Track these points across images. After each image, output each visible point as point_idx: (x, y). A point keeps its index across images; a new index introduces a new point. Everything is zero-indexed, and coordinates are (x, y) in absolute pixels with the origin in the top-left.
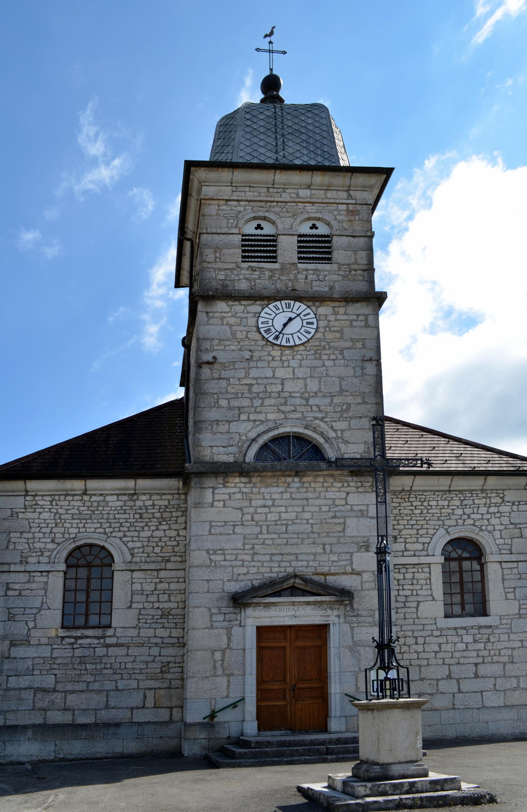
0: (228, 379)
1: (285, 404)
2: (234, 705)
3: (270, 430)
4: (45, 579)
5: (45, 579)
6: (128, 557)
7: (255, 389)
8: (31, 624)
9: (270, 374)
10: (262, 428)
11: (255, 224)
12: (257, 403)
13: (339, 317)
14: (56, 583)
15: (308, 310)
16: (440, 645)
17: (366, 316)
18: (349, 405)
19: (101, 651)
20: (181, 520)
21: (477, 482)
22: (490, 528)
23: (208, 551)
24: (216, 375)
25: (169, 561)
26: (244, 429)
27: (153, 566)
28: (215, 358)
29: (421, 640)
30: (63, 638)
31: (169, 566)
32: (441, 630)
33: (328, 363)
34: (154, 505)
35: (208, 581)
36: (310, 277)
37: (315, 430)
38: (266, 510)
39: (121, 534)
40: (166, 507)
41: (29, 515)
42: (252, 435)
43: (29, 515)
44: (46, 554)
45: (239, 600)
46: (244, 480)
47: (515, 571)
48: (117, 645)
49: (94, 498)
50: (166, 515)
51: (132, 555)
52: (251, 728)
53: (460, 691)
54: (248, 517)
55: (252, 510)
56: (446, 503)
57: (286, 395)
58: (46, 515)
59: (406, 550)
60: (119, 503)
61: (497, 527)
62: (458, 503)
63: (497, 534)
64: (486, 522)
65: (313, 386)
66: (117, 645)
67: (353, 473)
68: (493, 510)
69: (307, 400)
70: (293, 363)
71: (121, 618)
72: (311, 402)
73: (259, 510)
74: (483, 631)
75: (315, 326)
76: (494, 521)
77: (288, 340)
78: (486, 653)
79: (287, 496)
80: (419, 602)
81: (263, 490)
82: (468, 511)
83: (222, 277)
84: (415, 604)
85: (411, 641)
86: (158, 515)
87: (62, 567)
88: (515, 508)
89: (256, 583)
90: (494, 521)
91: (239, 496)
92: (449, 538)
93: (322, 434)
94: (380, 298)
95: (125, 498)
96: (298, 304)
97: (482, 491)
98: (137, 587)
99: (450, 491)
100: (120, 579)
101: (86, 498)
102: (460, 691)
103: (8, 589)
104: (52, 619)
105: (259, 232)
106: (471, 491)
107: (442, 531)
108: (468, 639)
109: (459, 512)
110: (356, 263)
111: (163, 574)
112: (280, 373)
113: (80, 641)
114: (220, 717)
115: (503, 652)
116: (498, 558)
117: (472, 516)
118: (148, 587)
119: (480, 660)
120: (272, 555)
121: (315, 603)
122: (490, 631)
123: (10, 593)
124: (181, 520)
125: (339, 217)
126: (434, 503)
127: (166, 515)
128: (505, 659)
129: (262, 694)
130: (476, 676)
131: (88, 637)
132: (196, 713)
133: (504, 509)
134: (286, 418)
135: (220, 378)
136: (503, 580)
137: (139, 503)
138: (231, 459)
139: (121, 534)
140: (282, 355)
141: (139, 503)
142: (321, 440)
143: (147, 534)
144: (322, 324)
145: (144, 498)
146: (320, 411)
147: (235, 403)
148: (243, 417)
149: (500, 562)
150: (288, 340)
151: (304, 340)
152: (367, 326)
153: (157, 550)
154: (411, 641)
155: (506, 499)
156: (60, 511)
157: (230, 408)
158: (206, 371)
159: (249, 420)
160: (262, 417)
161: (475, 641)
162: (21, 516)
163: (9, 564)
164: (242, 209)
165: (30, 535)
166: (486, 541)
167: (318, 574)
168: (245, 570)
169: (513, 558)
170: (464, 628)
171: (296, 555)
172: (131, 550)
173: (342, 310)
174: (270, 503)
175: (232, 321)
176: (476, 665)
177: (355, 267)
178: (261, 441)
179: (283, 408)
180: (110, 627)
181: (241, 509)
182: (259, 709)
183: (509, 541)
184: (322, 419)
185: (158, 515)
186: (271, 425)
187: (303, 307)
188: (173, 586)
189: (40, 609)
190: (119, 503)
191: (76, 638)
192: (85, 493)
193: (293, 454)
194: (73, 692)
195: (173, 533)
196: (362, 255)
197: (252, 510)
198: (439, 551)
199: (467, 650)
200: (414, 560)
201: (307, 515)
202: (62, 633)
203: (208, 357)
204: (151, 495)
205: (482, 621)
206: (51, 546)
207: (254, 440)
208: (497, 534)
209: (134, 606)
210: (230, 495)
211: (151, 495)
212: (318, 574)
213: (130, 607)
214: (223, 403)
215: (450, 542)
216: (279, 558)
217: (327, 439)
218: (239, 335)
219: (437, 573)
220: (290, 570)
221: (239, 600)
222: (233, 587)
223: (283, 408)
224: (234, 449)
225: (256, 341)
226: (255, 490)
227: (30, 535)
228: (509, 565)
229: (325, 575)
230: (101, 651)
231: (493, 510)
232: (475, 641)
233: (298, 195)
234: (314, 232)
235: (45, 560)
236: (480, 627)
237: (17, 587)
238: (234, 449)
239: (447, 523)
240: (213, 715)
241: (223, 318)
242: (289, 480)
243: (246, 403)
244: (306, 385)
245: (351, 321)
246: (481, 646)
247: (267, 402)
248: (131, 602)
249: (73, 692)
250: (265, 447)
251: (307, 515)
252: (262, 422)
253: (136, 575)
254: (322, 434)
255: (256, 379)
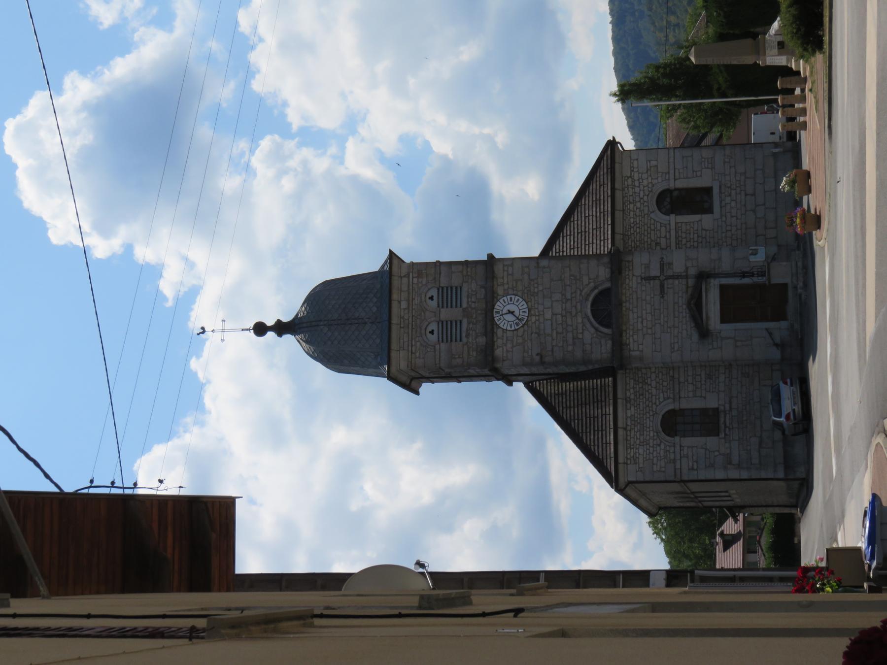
0: (553, 346)
1: (571, 313)
2: (770, 334)
3: (589, 320)
4: (686, 448)
5: (686, 448)
6: (670, 400)
7: (560, 330)
8: (716, 453)
9: (549, 322)
10: (588, 325)
11: (429, 335)
12: (570, 329)
13: (505, 281)
14: (688, 441)
15: (501, 300)
16: (732, 217)
17: (504, 266)
18: (571, 276)
19: (734, 413)
20: (644, 371)
21: (618, 194)
22: (650, 185)
23: (672, 352)
24: (550, 353)
25: (673, 377)
26: (588, 336)
27: (677, 386)
28: (537, 355)
29: (729, 228)
30: (726, 435)
31: (676, 376)
32: (722, 216)
33: (541, 288)
34: (634, 388)
35: (691, 351)
36: (473, 300)
37: (589, 295)
38: (645, 321)
39: (654, 406)
40: (635, 380)
41: (641, 460)
42: (593, 330)
43: (641, 460)
44: (668, 448)
45: (704, 333)
46: (624, 334)
47: (681, 171)
48: (730, 403)
49: (629, 423)
50: (640, 380)
51: (668, 398)
52: (784, 324)
53: (764, 204)
54: (649, 331)
55: (645, 329)
56: (632, 213)
57: (564, 312)
58: (641, 451)
59: (666, 237)
60: (632, 409)
61: (650, 180)
62: (632, 206)
63: (655, 181)
64: (646, 188)
65: (557, 296)
66: (730, 403)
67: (620, 273)
68: (637, 183)
69: (567, 300)
70: (541, 308)
71: (712, 402)
72: (569, 297)
73: (645, 325)
74: (723, 191)
75: (513, 297)
76: (645, 182)
77: (524, 312)
78: (738, 190)
79: (635, 310)
80: (703, 229)
81: (631, 323)
82: (638, 199)
83: (475, 354)
84: (704, 232)
85: (729, 234)
86: (641, 385)
87: (677, 439)
88: (636, 170)
89: (693, 325)
90: (645, 182)
91: (635, 337)
92: (657, 211)
93: (592, 290)
94: (491, 256)
95: (628, 405)
96: (496, 307)
97: (623, 190)
98: (691, 394)
99: (624, 210)
100: (685, 405)
101: (629, 428)
102: (764, 204)
103: (693, 469)
104: (712, 442)
105: (436, 332)
106: (623, 197)
107: (652, 215)
108: (728, 199)
109: (638, 204)
110: (462, 272)
111: (682, 379)
112: (548, 315)
113: (728, 424)
114: (778, 340)
115: (738, 179)
116: (672, 181)
117: (641, 196)
118: (691, 387)
119: (743, 193)
120: (674, 317)
121: (706, 293)
122: (723, 187)
123: (695, 467)
124: (644, 371)
125: (424, 282)
126: (632, 220)
127: (640, 380)
128: (743, 178)
129: (764, 319)
130: (754, 195)
131: (725, 421)
132: (776, 354)
133: (636, 176)
134: (581, 312)
135: (552, 351)
136: (687, 178)
137: (632, 397)
138: (610, 343)
139: (654, 406)
140: (535, 315)
141: (632, 397)
142: (596, 291)
143: (654, 391)
144: (510, 292)
145: (628, 394)
146: (575, 292)
147: (570, 341)
148: (580, 336)
149: (675, 180)
150: (524, 312)
151: (524, 302)
152: (512, 265)
153: (665, 384)
154: (729, 234)
155: (629, 175)
156: (638, 442)
157: (574, 344)
158: (547, 359)
159: (582, 333)
160: (580, 326)
161: (730, 195)
162: (641, 465)
163: (675, 469)
164: (418, 344)
165: (655, 459)
166: (661, 187)
167: (687, 291)
168: (684, 332)
169: (672, 172)
170: (721, 202)
171: (674, 303)
172: (665, 399)
173: (500, 281)
174: (640, 320)
175: (509, 346)
176: (746, 195)
177: (465, 273)
178: (597, 325)
179: (574, 314)
180: (718, 409)
181: (644, 335)
182: (772, 320)
183: (660, 175)
184: (581, 291)
185: (641, 385)
186: (586, 320)
187: (498, 303)
188: (690, 373)
189: (706, 449)
190: (632, 409)
191: (726, 427)
192: (625, 429)
193: (606, 308)
194: (762, 426)
195: (653, 376)
196: (454, 268)
197: (645, 329)
198: (667, 217)
199: (736, 201)
200: (673, 233)
201: (648, 298)
202: (722, 435)
203: (537, 359)
204: (626, 390)
205: (716, 191)
206: (663, 446)
207: (597, 330)
208: (655, 181)
209: (703, 395)
210: (634, 341)
211: (626, 390)
212: (687, 291)
213: (705, 398)
214: (570, 348)
215: (660, 209)
216: (676, 313)
217: (595, 288)
218: (520, 340)
219: (682, 219)
220: (684, 307)
221: (704, 333)
222: (695, 337)
223: (574, 314)
224: (603, 341)
225: (524, 331)
226: (631, 327)
227: (655, 459)
228: (677, 174)
229: (687, 287)
230: (734, 413)
231: (637, 183)
232: (730, 195)
233: (405, 309)
234: (435, 298)
235: (672, 450)
236: (720, 192)
237: (691, 464)
238: (603, 341)
239: (646, 212)
240: (776, 345)
241: (507, 351)
242: (624, 309)
243: (570, 335)
244: (557, 301)
245: (508, 275)
246: (733, 192)
247: (569, 322)
248: (701, 397)
249: (762, 426)
250: (600, 323)
251: (648, 298)
252: (584, 325)
253: (682, 395)
254: (592, 290)
255: (552, 330)
